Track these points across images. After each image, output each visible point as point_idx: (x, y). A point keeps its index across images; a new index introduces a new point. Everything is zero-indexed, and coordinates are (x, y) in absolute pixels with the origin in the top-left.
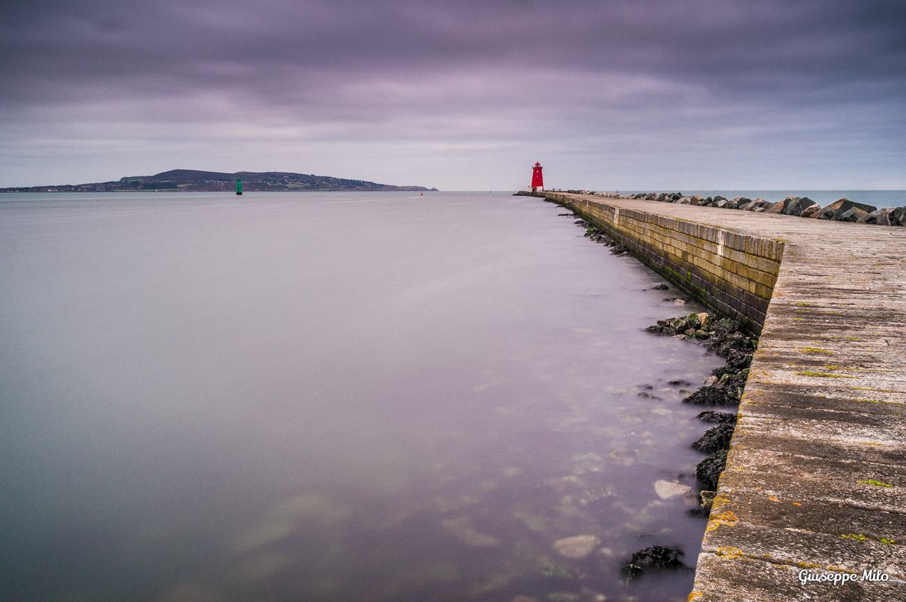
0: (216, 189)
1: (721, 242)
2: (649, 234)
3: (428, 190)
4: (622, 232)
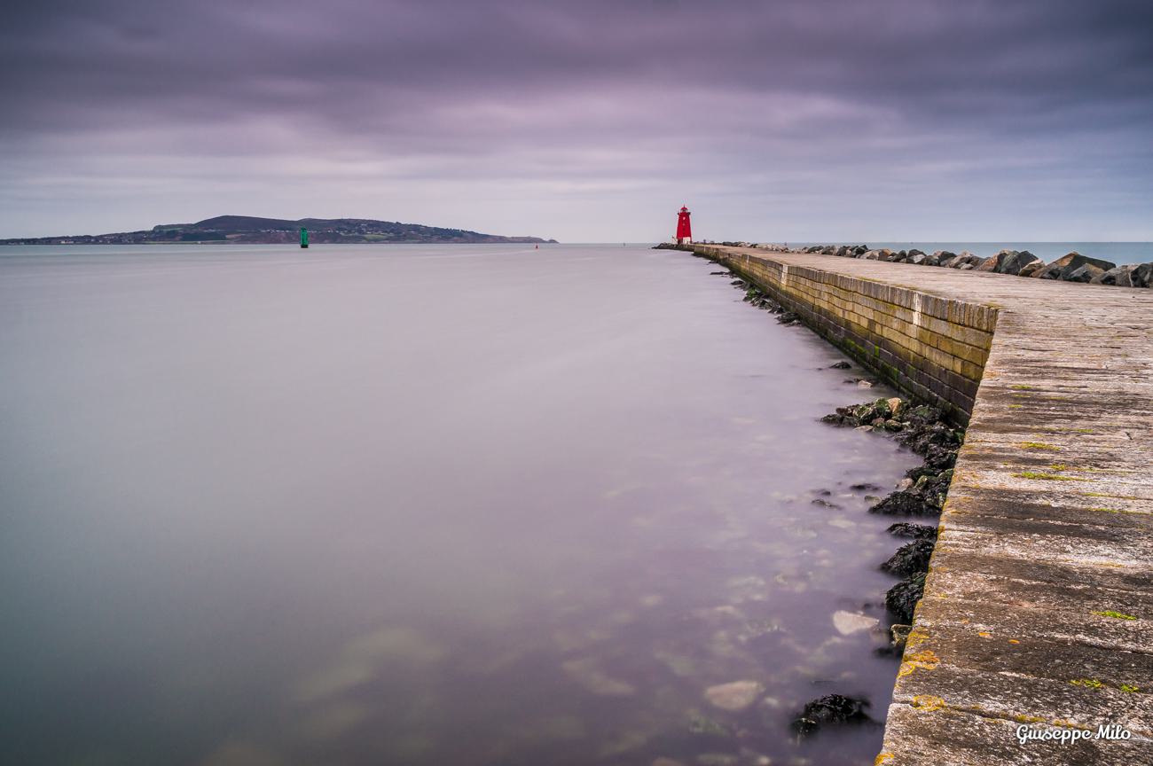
1: (918, 308)
2: (826, 297)
3: (544, 242)
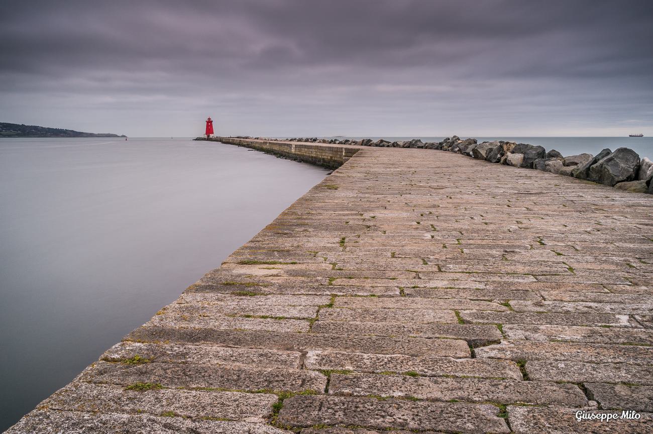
0: (70, 136)
1: (344, 151)
2: (315, 153)
3: (119, 137)
4: (298, 155)
